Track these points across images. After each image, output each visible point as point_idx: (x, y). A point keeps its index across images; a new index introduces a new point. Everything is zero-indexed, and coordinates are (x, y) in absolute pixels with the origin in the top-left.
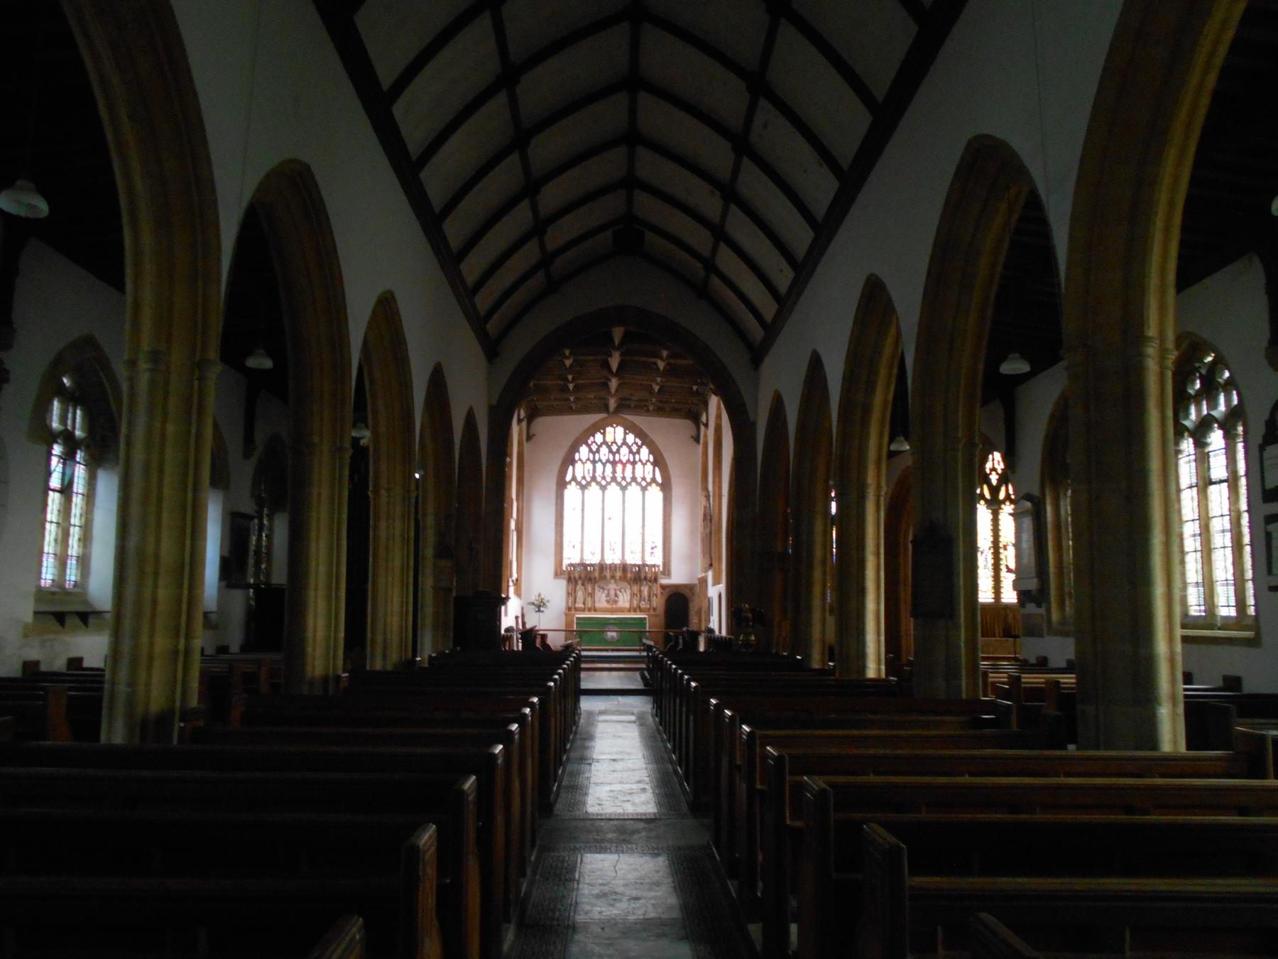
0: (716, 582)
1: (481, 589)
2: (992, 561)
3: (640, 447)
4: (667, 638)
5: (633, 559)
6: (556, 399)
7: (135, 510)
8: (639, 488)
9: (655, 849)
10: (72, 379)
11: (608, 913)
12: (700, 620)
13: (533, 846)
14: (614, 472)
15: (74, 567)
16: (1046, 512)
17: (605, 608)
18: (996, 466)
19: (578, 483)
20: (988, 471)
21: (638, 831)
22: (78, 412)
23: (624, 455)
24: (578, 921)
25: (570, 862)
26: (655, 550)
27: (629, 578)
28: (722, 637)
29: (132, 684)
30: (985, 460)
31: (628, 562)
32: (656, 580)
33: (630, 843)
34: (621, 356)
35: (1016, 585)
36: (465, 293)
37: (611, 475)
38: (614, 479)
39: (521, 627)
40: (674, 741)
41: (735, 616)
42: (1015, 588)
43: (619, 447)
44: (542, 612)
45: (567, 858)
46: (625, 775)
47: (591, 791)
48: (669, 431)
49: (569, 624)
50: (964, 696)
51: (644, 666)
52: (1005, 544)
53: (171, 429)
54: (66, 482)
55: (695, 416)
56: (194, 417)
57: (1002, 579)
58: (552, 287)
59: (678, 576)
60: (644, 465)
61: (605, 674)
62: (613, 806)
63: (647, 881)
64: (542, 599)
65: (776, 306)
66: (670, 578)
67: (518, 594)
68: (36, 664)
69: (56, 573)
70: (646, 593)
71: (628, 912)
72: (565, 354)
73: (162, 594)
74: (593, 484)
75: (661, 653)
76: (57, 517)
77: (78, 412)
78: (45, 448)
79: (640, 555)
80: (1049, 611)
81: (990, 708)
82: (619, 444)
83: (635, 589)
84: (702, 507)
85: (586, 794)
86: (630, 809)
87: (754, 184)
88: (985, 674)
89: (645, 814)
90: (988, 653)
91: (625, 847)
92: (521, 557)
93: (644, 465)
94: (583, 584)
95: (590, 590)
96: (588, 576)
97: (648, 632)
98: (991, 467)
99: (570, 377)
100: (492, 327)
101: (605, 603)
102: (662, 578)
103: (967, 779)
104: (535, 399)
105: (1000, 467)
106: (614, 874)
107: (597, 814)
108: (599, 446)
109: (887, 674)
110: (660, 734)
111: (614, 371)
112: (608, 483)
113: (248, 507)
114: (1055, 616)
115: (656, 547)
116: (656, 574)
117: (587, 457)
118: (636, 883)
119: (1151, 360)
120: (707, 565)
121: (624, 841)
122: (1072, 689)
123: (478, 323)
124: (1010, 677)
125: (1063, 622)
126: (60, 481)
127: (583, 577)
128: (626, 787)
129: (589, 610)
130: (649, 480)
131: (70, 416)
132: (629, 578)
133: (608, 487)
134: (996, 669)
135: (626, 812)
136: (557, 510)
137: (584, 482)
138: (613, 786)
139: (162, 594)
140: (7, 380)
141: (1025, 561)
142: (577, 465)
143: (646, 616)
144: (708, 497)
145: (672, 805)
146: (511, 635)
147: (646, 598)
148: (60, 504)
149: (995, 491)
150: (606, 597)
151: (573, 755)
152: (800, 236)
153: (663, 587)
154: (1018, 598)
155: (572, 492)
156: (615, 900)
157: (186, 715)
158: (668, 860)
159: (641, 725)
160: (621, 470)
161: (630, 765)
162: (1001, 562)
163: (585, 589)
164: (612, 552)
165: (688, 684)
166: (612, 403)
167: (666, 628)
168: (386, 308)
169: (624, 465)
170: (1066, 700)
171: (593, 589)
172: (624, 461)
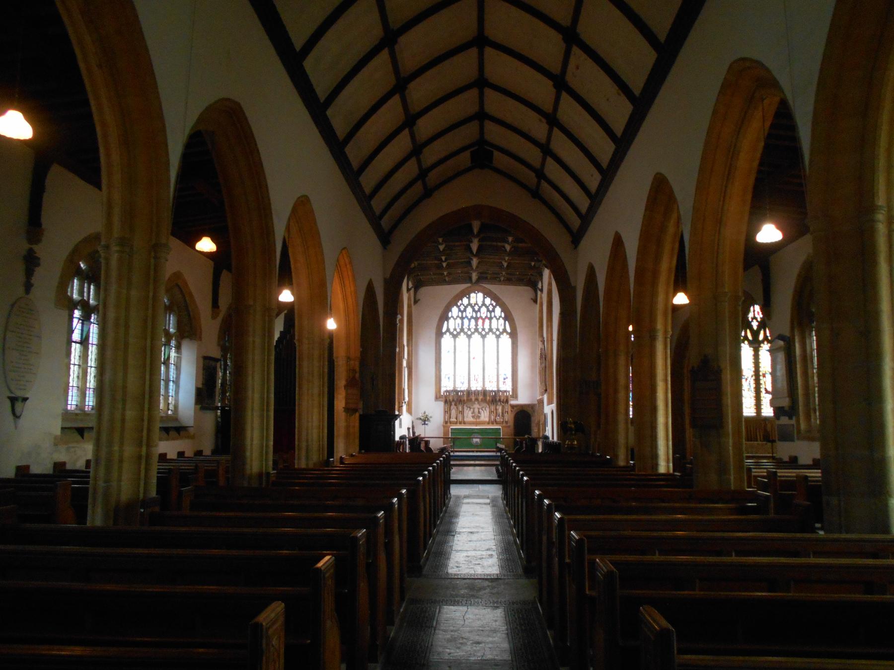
0: (550, 402)
1: (381, 409)
2: (754, 386)
3: (494, 307)
4: (516, 443)
5: (491, 386)
6: (434, 274)
7: (109, 353)
8: (494, 336)
9: (496, 603)
10: (85, 262)
11: (456, 654)
12: (539, 430)
13: (402, 599)
14: (477, 325)
15: (91, 395)
16: (795, 349)
17: (470, 422)
18: (757, 316)
19: (451, 333)
20: (750, 320)
21: (484, 588)
22: (92, 287)
23: (484, 313)
24: (432, 660)
26: (506, 380)
27: (488, 400)
28: (553, 442)
29: (107, 481)
30: (748, 311)
31: (487, 389)
32: (507, 401)
33: (477, 598)
34: (479, 241)
35: (772, 403)
36: (364, 199)
37: (474, 327)
38: (476, 330)
39: (412, 435)
40: (515, 519)
41: (563, 427)
42: (771, 406)
43: (480, 308)
44: (427, 424)
45: (429, 609)
46: (478, 544)
47: (452, 556)
48: (517, 295)
49: (446, 433)
50: (732, 488)
51: (498, 463)
52: (764, 372)
53: (134, 293)
54: (84, 336)
55: (533, 284)
56: (151, 286)
57: (762, 399)
58: (428, 193)
59: (523, 399)
60: (498, 319)
61: (471, 468)
62: (467, 568)
63: (487, 628)
64: (427, 416)
65: (589, 201)
66: (518, 400)
67: (409, 411)
68: (64, 464)
69: (79, 400)
70: (500, 411)
71: (471, 654)
72: (439, 242)
73: (130, 414)
74: (462, 334)
75: (507, 454)
76: (78, 361)
77: (92, 287)
78: (66, 313)
79: (496, 384)
80: (798, 421)
81: (754, 497)
82: (480, 305)
83: (493, 408)
84: (540, 348)
85: (448, 559)
86: (479, 571)
87: (569, 111)
88: (749, 470)
89: (490, 575)
90: (752, 453)
91: (472, 600)
92: (411, 387)
93: (498, 319)
94: (455, 405)
95: (460, 408)
96: (459, 399)
97: (503, 438)
98: (753, 316)
99: (443, 258)
100: (385, 223)
101: (471, 418)
102: (511, 400)
103: (734, 558)
104: (419, 274)
105: (760, 316)
106: (462, 623)
107: (455, 575)
108: (466, 307)
109: (674, 470)
110: (506, 513)
111: (475, 253)
112: (473, 333)
113: (216, 353)
114: (803, 426)
115: (507, 378)
116: (507, 397)
117: (457, 315)
118: (479, 630)
119: (881, 224)
120: (543, 391)
121: (473, 596)
122: (817, 481)
123: (374, 220)
124: (768, 472)
125: (809, 431)
126: (80, 335)
127: (455, 400)
128: (479, 553)
129: (460, 423)
130: (501, 330)
131: (86, 290)
132: (488, 400)
133: (473, 336)
134: (758, 465)
135: (476, 573)
136: (436, 353)
137: (455, 333)
138: (468, 552)
139: (130, 414)
140: (38, 265)
141: (779, 385)
142: (450, 321)
143: (500, 427)
144: (543, 342)
145: (511, 568)
146: (403, 441)
147: (501, 415)
148: (80, 351)
149: (755, 334)
150: (472, 413)
151: (441, 528)
152: (604, 149)
153: (513, 406)
154: (774, 413)
155: (447, 340)
156: (462, 644)
157: (145, 503)
158: (504, 611)
159: (494, 506)
160: (482, 324)
161: (482, 537)
162: (761, 386)
163: (457, 408)
164: (475, 382)
165: (522, 478)
166: (474, 276)
167: (515, 435)
168: (302, 206)
169: (484, 320)
170: (814, 491)
171: (463, 408)
172: (484, 317)
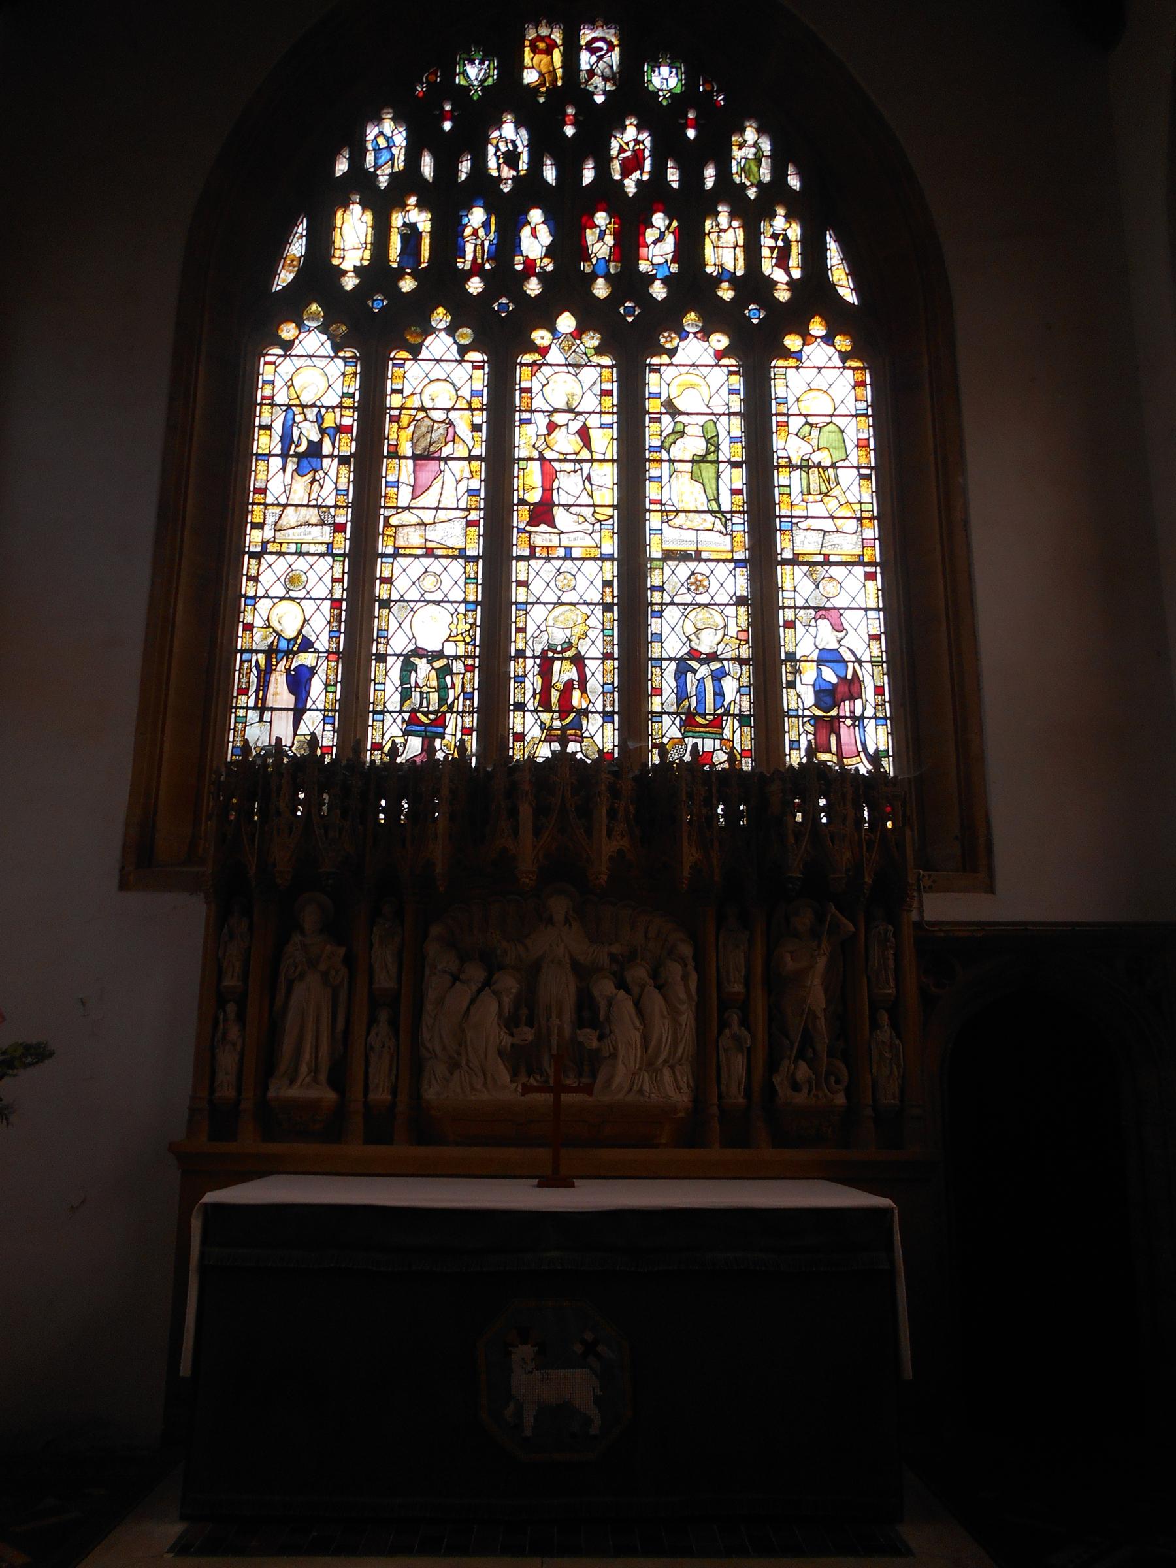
25: (270, 558)
150: (510, 1023)
